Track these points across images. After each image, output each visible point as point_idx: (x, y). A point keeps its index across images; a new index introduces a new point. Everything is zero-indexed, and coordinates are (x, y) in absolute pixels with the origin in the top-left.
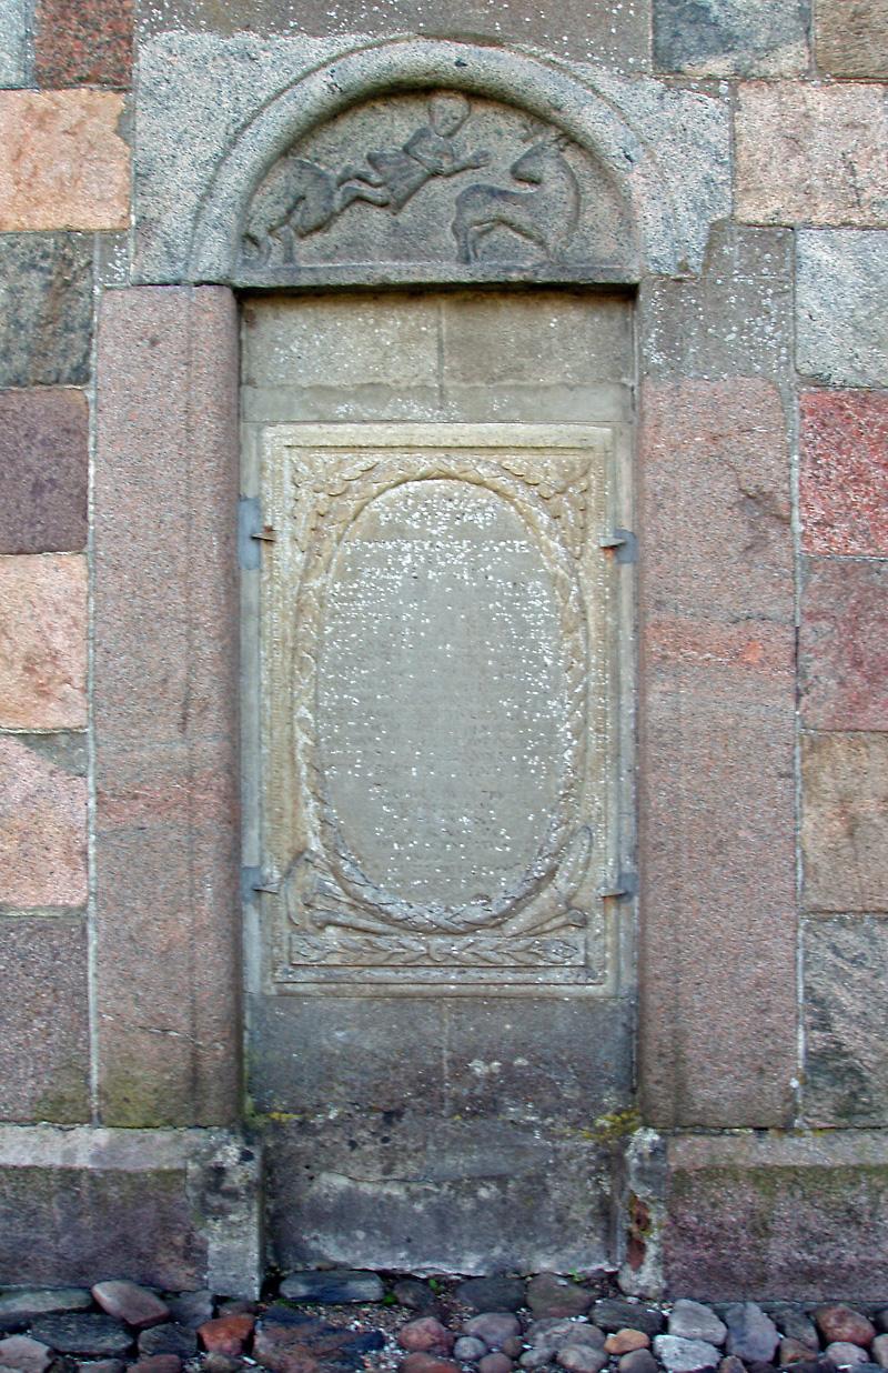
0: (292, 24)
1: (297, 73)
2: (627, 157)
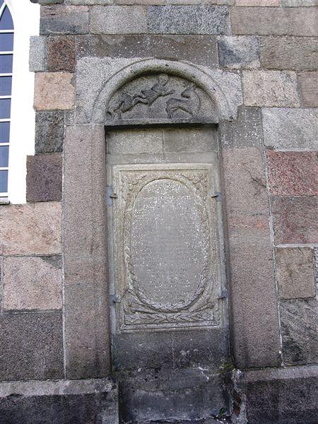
1: (122, 67)
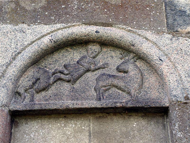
0: (39, 21)
1: (39, 36)
2: (160, 60)
